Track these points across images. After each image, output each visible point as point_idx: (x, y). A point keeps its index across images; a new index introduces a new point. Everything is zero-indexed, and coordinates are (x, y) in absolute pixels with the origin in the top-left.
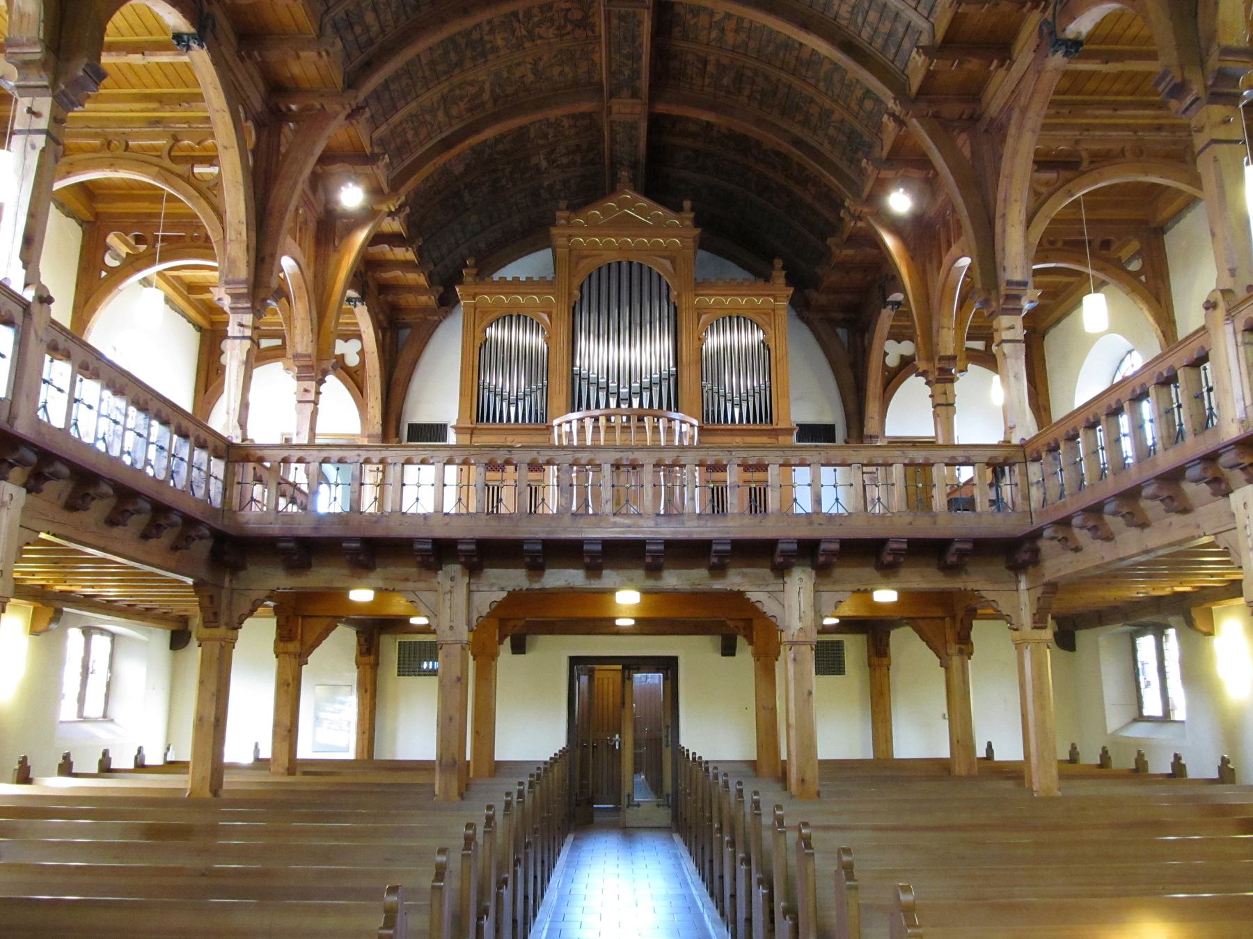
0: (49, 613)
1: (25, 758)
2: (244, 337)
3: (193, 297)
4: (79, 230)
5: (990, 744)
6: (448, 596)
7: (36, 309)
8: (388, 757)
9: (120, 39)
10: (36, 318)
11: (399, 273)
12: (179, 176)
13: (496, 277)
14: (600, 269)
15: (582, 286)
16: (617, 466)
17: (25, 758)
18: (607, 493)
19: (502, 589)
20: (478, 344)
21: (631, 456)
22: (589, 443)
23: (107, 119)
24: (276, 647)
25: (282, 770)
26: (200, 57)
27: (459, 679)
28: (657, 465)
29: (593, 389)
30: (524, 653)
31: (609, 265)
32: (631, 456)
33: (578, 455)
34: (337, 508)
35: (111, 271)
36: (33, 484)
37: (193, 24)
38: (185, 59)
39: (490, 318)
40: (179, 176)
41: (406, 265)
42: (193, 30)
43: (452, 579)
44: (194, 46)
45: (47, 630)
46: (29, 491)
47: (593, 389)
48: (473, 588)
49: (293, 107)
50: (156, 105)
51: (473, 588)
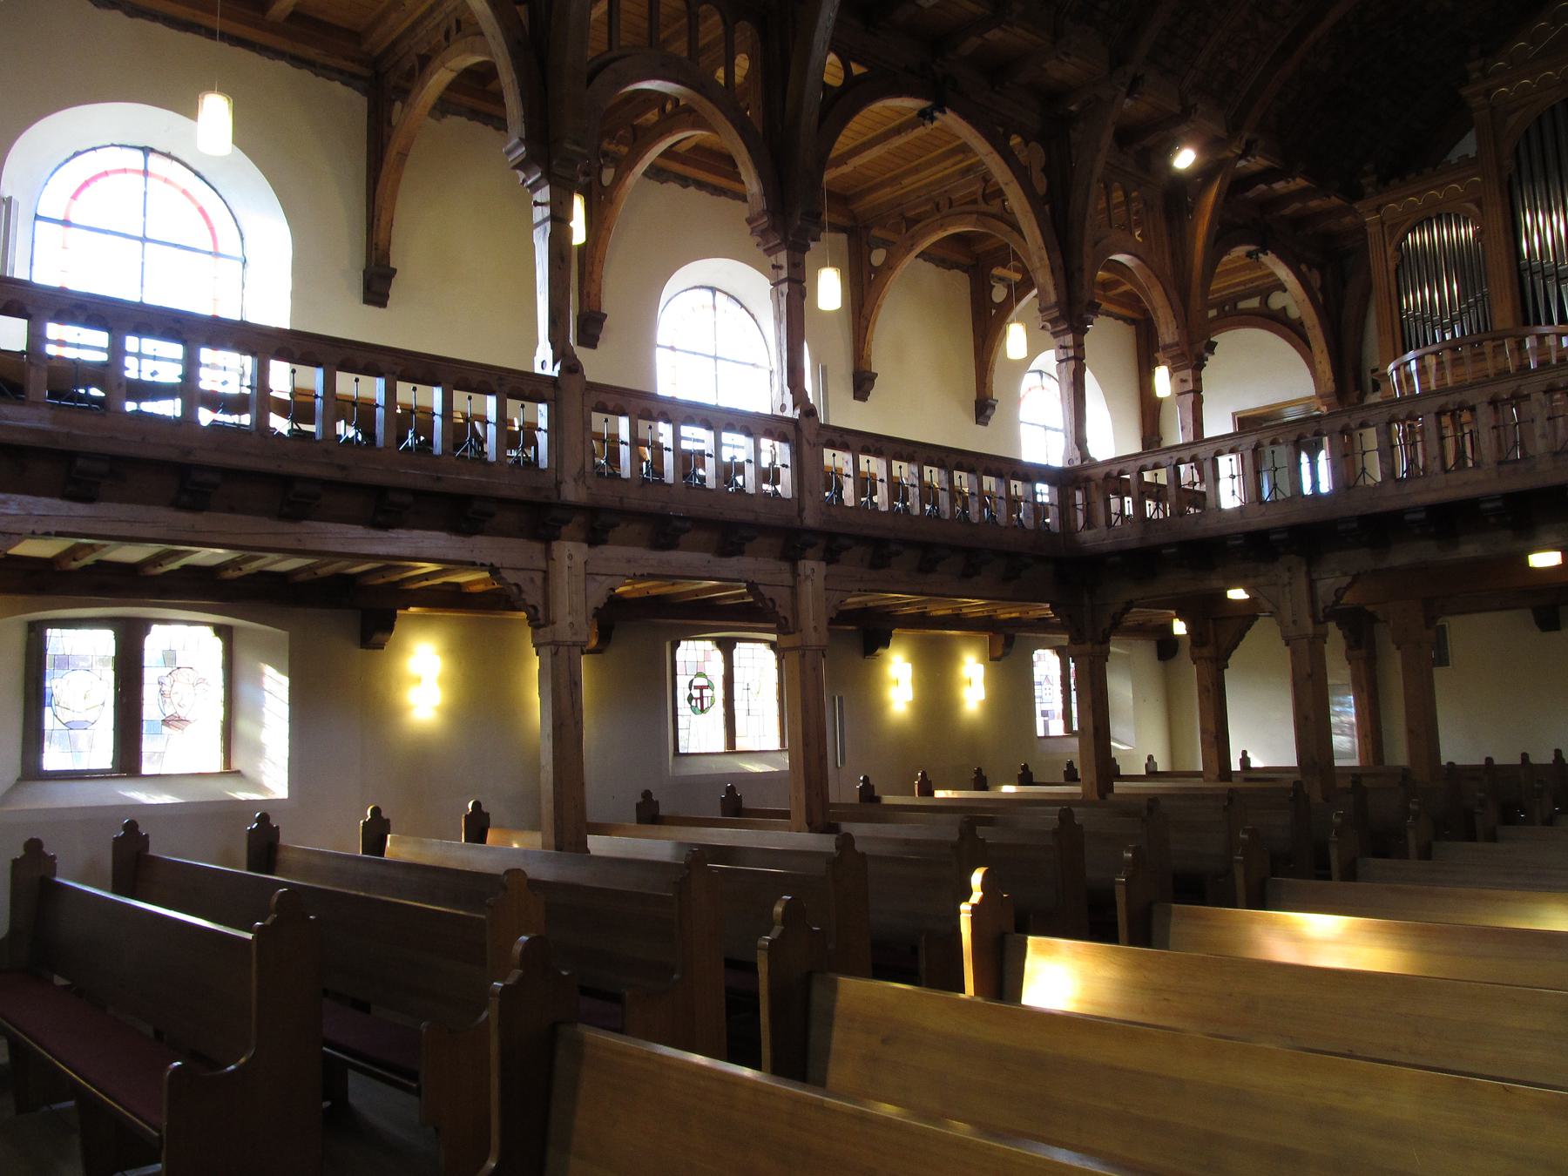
0: (1001, 639)
1: (979, 770)
2: (1068, 359)
3: (1110, 294)
4: (966, 276)
5: (1244, 753)
6: (1287, 589)
7: (805, 424)
8: (63, 804)
9: (903, 119)
10: (806, 432)
11: (1297, 205)
12: (993, 216)
13: (1453, 157)
14: (1539, 118)
15: (1517, 149)
16: (1494, 402)
17: (979, 770)
18: (1487, 438)
19: (1345, 574)
20: (1392, 266)
21: (1458, 397)
22: (1433, 387)
23: (931, 184)
24: (1192, 654)
25: (1214, 777)
26: (949, 120)
27: (1310, 676)
28: (1439, 414)
29: (1551, 283)
30: (1558, 628)
31: (1553, 109)
32: (1458, 397)
33: (1395, 411)
34: (1237, 504)
35: (1000, 306)
36: (830, 557)
37: (927, 99)
38: (936, 124)
39: (1403, 229)
40: (993, 216)
41: (1302, 194)
42: (929, 103)
43: (1289, 570)
44: (937, 114)
45: (1004, 655)
46: (828, 563)
47: (1551, 283)
48: (1315, 576)
49: (1073, 108)
50: (959, 158)
51: (1315, 576)
